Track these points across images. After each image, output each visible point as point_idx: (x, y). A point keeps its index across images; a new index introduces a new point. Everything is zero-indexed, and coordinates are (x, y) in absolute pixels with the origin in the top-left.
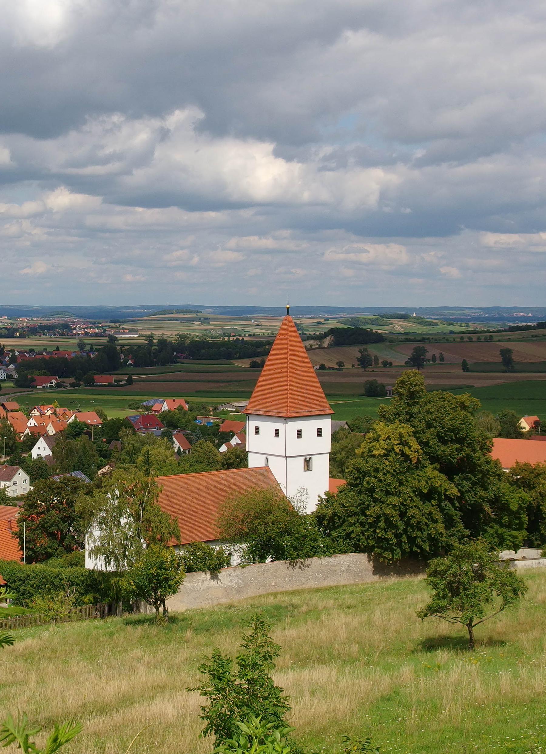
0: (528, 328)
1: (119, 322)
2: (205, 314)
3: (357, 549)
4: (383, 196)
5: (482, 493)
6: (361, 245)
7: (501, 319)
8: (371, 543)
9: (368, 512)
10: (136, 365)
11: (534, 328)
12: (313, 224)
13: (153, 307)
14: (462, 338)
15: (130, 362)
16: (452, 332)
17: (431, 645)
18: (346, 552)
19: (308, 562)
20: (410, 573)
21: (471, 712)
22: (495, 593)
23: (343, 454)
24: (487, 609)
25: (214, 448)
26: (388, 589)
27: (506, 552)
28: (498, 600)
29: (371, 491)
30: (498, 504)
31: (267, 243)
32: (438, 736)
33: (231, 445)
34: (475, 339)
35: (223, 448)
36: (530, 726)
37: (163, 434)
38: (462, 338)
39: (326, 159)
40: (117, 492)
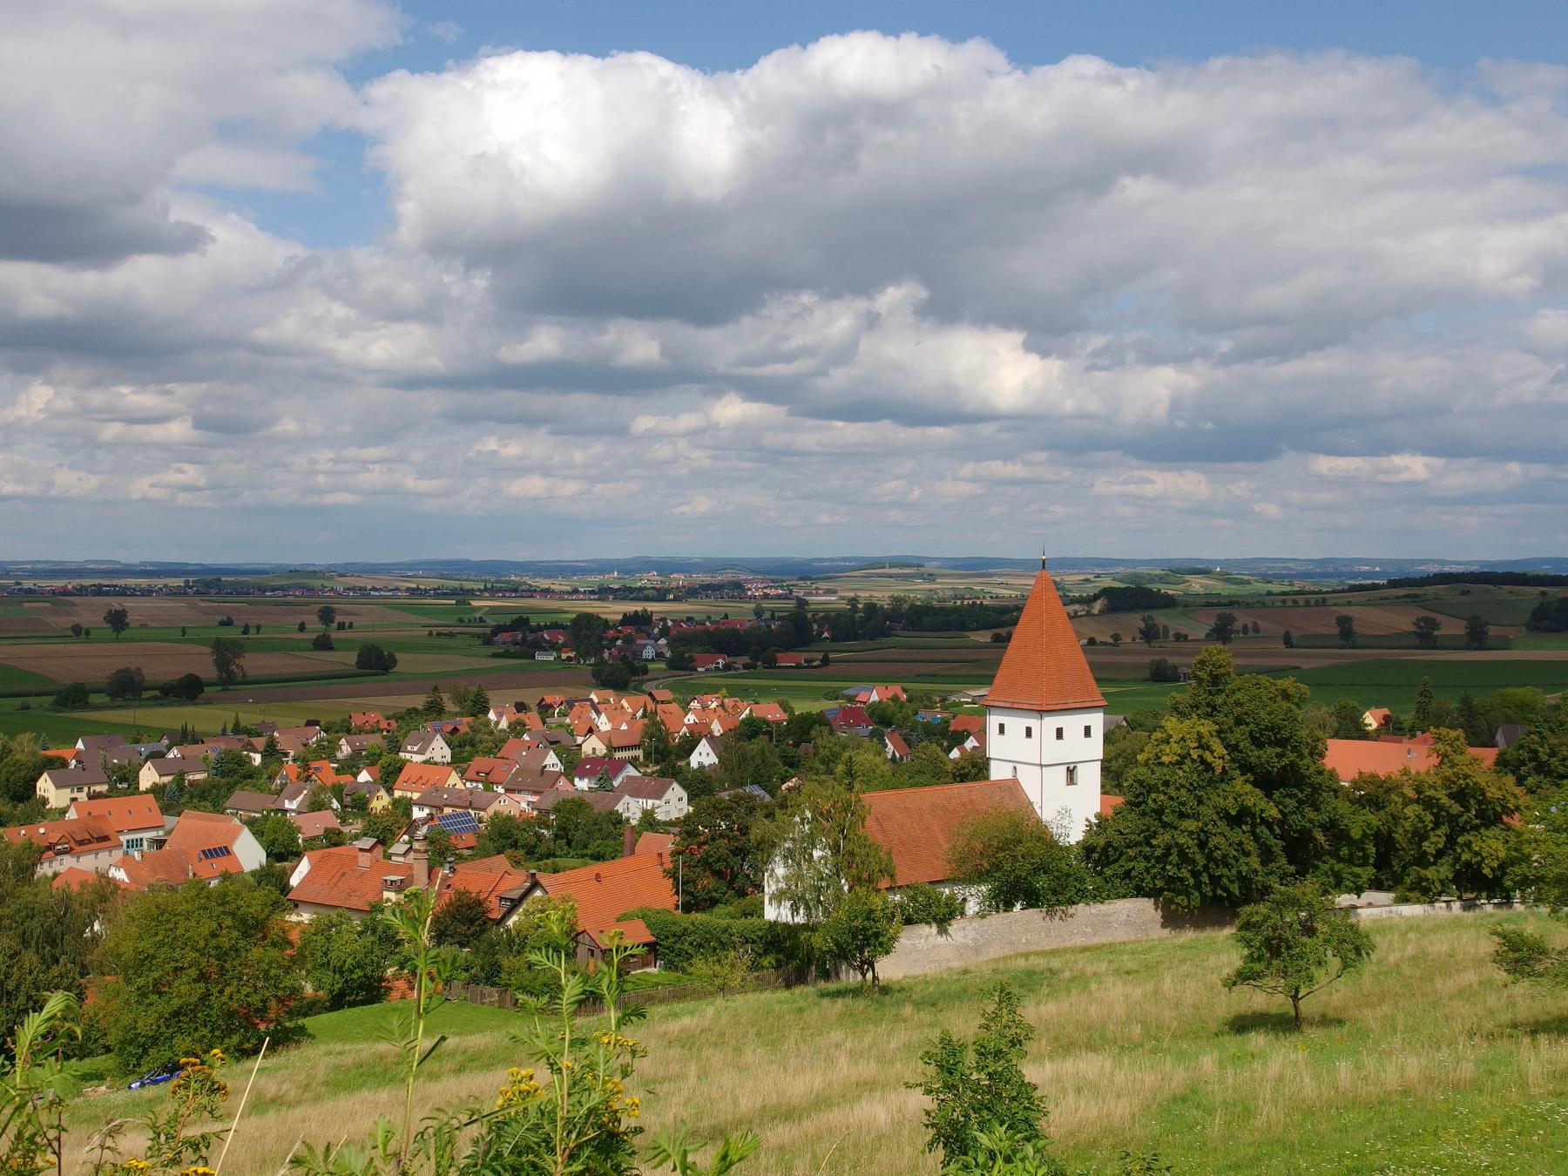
0: (1375, 587)
3: (1140, 892)
4: (1175, 406)
5: (1312, 815)
6: (1144, 473)
8: (1159, 884)
9: (1154, 842)
10: (833, 639)
11: (1383, 587)
14: (1284, 602)
16: (1270, 593)
17: (1242, 1024)
21: (1297, 1117)
22: (1329, 953)
25: (941, 754)
26: (1182, 947)
28: (1335, 963)
29: (1159, 812)
30: (1336, 831)
31: (1015, 470)
32: (1251, 1151)
36: (1378, 1137)
37: (872, 734)
39: (1096, 353)
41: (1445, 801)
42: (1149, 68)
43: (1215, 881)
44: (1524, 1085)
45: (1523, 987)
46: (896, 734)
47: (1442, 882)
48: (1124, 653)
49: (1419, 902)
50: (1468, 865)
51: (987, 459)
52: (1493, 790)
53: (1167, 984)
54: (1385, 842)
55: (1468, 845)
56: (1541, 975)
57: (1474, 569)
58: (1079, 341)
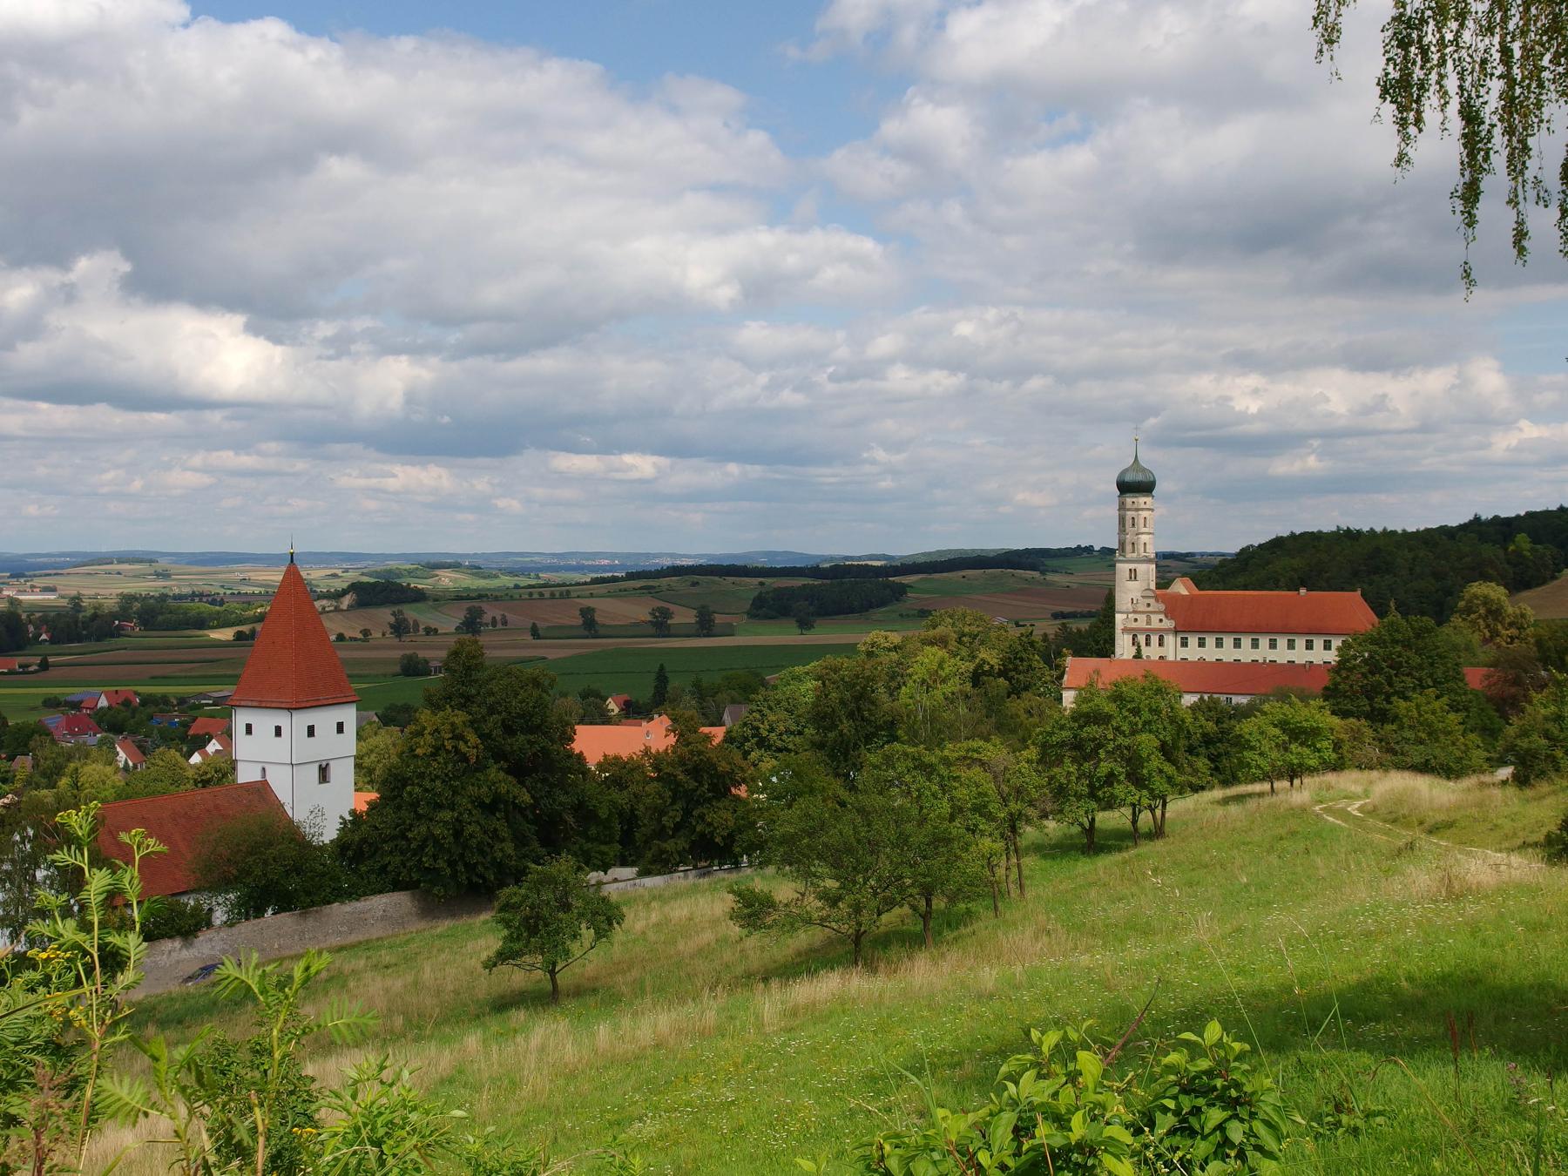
0: (614, 579)
1: (23, 576)
2: (162, 564)
3: (397, 886)
4: (410, 398)
5: (563, 798)
6: (387, 467)
7: (579, 568)
8: (415, 876)
9: (410, 835)
10: (53, 641)
11: (622, 579)
12: (319, 434)
13: (85, 554)
14: (531, 594)
15: (44, 637)
16: (517, 587)
17: (503, 1004)
18: (381, 892)
19: (327, 909)
20: (469, 913)
21: (561, 1082)
22: (583, 926)
23: (373, 756)
24: (575, 948)
25: (181, 759)
26: (440, 936)
27: (594, 874)
28: (588, 934)
29: (414, 805)
30: (585, 813)
31: (247, 461)
32: (519, 1120)
33: (207, 754)
34: (547, 595)
35: (196, 759)
36: (635, 1090)
37: (102, 742)
38: (531, 594)
39: (327, 342)
40: (31, 832)
41: (681, 777)
42: (334, 40)
43: (470, 868)
44: (760, 1025)
45: (753, 941)
46: (129, 741)
47: (679, 853)
48: (376, 648)
49: (659, 874)
50: (702, 835)
51: (218, 449)
52: (723, 763)
53: (427, 975)
54: (629, 820)
55: (702, 817)
56: (770, 927)
57: (702, 561)
58: (305, 330)
